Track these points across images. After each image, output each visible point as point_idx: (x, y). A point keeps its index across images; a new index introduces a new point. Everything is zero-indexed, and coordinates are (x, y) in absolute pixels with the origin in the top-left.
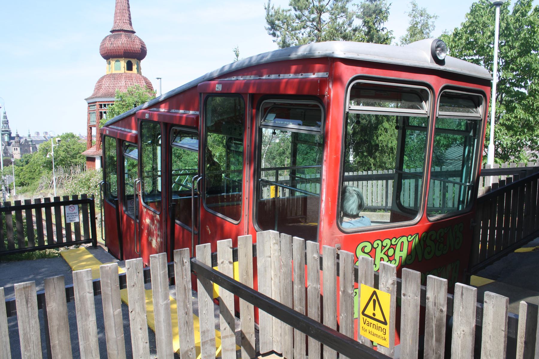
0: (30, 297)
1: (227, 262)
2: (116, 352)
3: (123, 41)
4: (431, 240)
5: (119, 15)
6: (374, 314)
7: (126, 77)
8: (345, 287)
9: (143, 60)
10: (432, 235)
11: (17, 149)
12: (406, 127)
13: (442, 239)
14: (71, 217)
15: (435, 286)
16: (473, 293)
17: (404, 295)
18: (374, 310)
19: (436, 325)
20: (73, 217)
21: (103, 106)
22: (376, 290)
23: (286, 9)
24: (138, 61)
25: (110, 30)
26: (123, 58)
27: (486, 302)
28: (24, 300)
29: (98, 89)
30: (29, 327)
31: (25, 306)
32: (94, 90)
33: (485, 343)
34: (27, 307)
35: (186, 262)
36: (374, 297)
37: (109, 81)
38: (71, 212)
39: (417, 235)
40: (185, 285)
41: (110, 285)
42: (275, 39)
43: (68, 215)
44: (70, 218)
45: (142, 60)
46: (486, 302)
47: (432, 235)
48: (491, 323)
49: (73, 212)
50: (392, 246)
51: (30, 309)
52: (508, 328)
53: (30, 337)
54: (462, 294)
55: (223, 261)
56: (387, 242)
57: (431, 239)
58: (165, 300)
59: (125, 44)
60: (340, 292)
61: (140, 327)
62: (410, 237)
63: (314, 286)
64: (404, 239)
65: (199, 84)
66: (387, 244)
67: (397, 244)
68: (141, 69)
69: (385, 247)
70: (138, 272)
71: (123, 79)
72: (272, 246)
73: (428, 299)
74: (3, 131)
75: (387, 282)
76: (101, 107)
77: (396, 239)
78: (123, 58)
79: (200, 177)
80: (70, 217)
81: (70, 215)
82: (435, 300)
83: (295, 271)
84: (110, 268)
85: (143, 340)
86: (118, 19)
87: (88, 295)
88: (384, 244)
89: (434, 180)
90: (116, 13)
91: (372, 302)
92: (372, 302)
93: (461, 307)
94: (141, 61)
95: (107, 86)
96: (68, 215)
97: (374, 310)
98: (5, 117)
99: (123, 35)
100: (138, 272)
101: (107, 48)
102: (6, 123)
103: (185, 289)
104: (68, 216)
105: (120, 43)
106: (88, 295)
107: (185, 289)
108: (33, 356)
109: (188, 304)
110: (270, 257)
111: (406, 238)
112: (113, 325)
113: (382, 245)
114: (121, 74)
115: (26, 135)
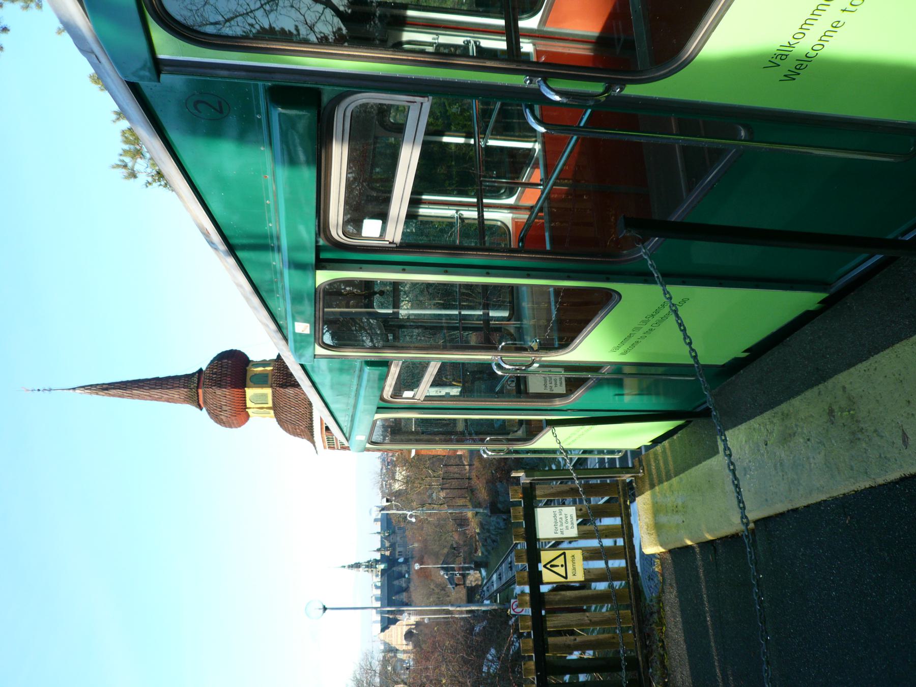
9: (249, 355)
11: (399, 552)
14: (565, 525)
20: (564, 520)
24: (251, 364)
25: (198, 410)
36: (548, 566)
43: (559, 531)
44: (567, 528)
68: (264, 361)
74: (383, 509)
80: (564, 527)
81: (559, 528)
89: (380, 581)
90: (168, 401)
91: (552, 569)
92: (552, 569)
94: (250, 359)
96: (559, 531)
98: (351, 567)
102: (357, 566)
104: (562, 533)
115: (379, 537)
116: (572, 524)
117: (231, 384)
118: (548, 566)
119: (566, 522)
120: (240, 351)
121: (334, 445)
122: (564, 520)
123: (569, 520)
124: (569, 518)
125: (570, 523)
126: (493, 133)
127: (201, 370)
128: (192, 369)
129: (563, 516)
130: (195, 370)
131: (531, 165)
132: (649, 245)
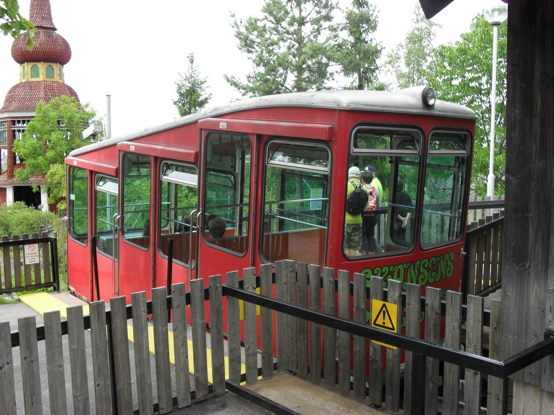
0: (100, 314)
1: (251, 288)
2: (163, 364)
3: (42, 40)
4: (423, 273)
5: (37, 8)
6: (384, 323)
7: (46, 86)
8: (358, 303)
9: (67, 64)
10: (425, 263)
12: (398, 162)
13: (434, 267)
14: (31, 258)
15: (432, 294)
16: (460, 296)
17: (408, 304)
18: (384, 319)
19: (433, 325)
20: (33, 258)
21: (16, 123)
22: (385, 303)
23: (255, 17)
24: (61, 66)
26: (42, 62)
27: (469, 303)
28: (97, 316)
29: (9, 101)
30: (100, 339)
31: (97, 322)
32: (4, 103)
33: (468, 333)
34: (99, 322)
35: (219, 287)
36: (384, 309)
37: (24, 91)
38: (31, 252)
39: (411, 264)
40: (217, 308)
41: (159, 305)
42: (250, 55)
43: (28, 255)
45: (65, 64)
46: (469, 303)
47: (425, 263)
48: (472, 318)
49: (33, 252)
50: (390, 273)
51: (100, 323)
52: (484, 320)
53: (100, 347)
54: (452, 299)
55: (248, 287)
56: (385, 269)
57: (424, 267)
58: (202, 320)
59: (44, 45)
60: (354, 309)
61: (181, 343)
62: (405, 264)
63: (330, 306)
64: (401, 267)
65: (200, 120)
66: (385, 271)
67: (394, 271)
68: (63, 76)
69: (384, 273)
70: (182, 295)
71: (42, 88)
72: (288, 273)
73: (427, 305)
75: (394, 295)
76: (14, 124)
77: (394, 267)
78: (42, 62)
79: (199, 212)
80: (30, 258)
81: (29, 255)
82: (432, 306)
83: (311, 294)
84: (160, 291)
85: (184, 355)
86: (36, 12)
87: (143, 313)
88: (383, 271)
91: (382, 312)
92: (382, 312)
93: (451, 309)
95: (21, 97)
96: (28, 255)
97: (384, 319)
99: (41, 33)
100: (182, 295)
101: (21, 49)
103: (218, 311)
104: (27, 257)
105: (39, 43)
106: (143, 313)
107: (218, 311)
108: (102, 364)
109: (219, 324)
110: (286, 284)
111: (402, 265)
112: (161, 340)
113: (382, 272)
114: (39, 82)
116: (31, 262)
117: (32, 54)
118: (384, 309)
119: (32, 259)
120: (70, 58)
121: (2, 126)
122: (33, 258)
123: (33, 260)
124: (34, 260)
125: (32, 260)
126: (112, 198)
127: (55, 29)
128: (57, 22)
129: (35, 257)
130: (56, 25)
131: (239, 240)
132: (420, 341)
